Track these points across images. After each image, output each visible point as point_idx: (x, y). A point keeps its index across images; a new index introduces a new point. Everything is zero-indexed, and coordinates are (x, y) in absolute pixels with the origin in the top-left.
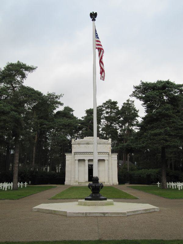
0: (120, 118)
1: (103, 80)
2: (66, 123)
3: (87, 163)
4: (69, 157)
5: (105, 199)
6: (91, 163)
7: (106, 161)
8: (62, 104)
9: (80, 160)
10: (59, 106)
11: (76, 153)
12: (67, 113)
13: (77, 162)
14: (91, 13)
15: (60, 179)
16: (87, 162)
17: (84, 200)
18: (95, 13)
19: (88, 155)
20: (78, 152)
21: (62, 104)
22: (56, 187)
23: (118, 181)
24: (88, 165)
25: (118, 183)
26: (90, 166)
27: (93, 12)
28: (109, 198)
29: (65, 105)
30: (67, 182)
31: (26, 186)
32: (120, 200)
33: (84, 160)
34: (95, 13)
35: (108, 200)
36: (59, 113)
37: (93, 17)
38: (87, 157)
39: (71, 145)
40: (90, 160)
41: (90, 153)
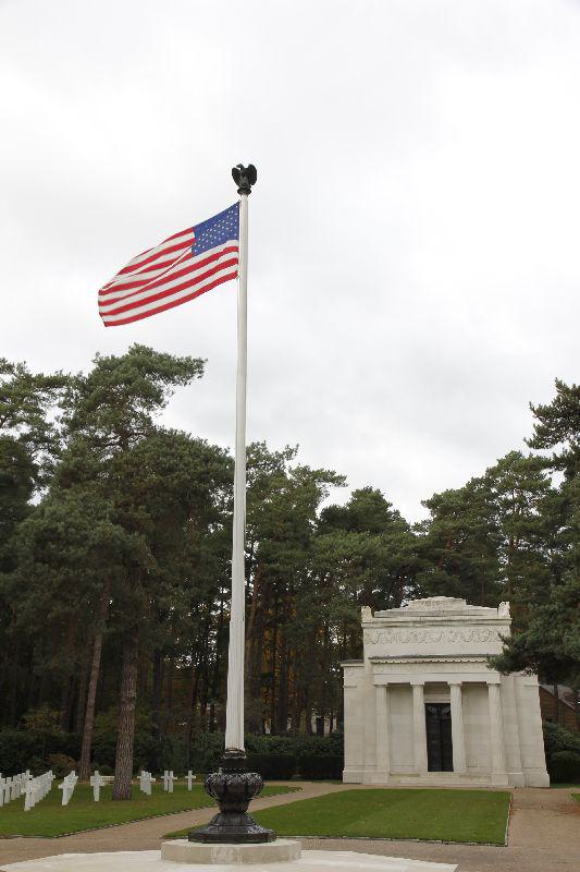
0: (298, 506)
1: (200, 363)
2: (345, 547)
3: (419, 700)
4: (354, 678)
5: (264, 838)
6: (439, 699)
7: (492, 691)
8: (338, 481)
9: (392, 688)
10: (329, 487)
11: (377, 661)
12: (370, 510)
13: (382, 693)
14: (234, 171)
15: (326, 762)
16: (418, 694)
17: (183, 843)
18: (246, 166)
19: (457, 668)
20: (409, 654)
21: (338, 481)
22: (298, 789)
23: (549, 769)
24: (427, 705)
25: (547, 777)
26: (434, 710)
27: (240, 166)
28: (282, 836)
29: (356, 483)
30: (346, 779)
31: (190, 788)
32: (103, 835)
33: (407, 688)
34: (246, 166)
35: (280, 842)
36: (331, 513)
37: (244, 180)
38: (419, 676)
39: (362, 630)
40: (429, 688)
41: (429, 660)
